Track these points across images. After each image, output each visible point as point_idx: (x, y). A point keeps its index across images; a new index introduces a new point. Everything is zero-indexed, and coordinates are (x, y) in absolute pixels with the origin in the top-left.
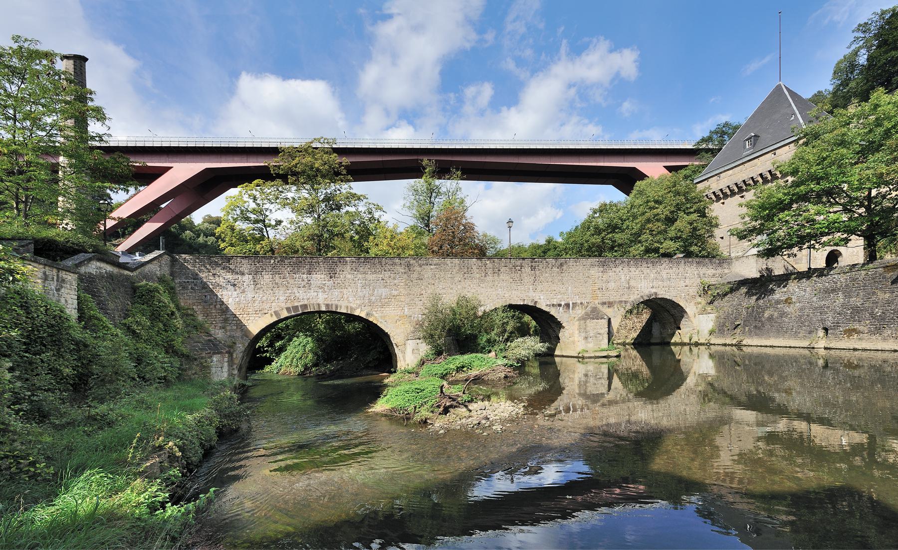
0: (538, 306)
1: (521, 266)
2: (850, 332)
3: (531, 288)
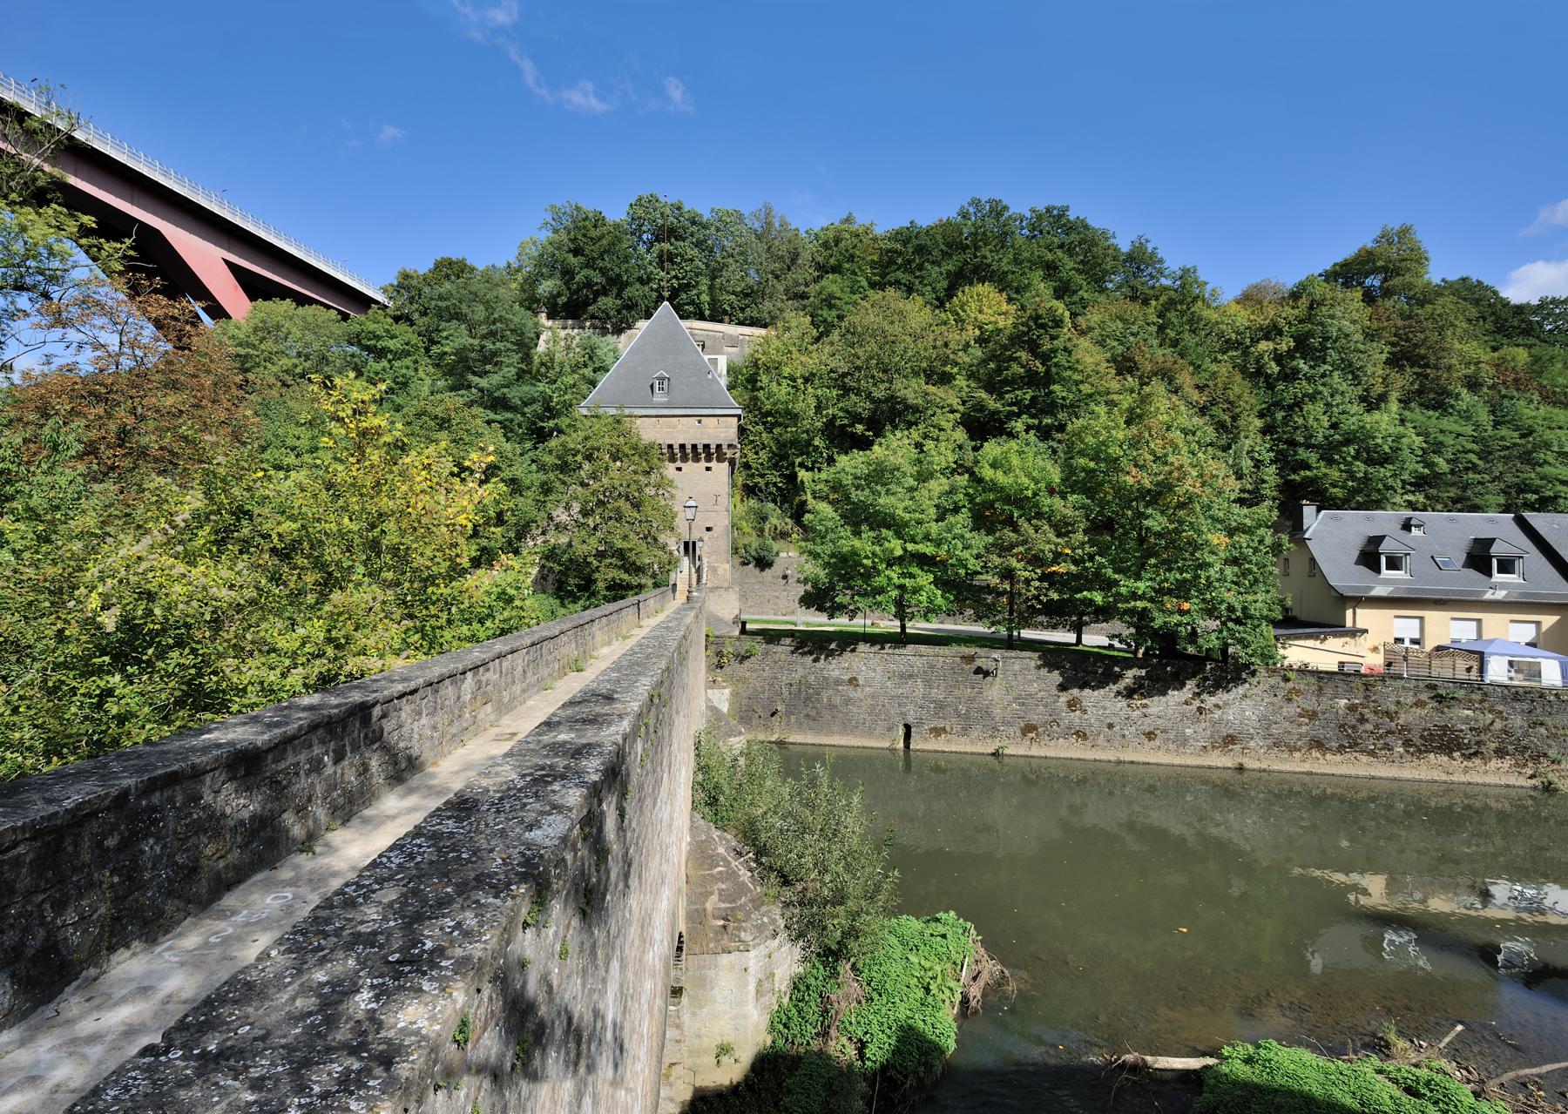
2: (938, 732)
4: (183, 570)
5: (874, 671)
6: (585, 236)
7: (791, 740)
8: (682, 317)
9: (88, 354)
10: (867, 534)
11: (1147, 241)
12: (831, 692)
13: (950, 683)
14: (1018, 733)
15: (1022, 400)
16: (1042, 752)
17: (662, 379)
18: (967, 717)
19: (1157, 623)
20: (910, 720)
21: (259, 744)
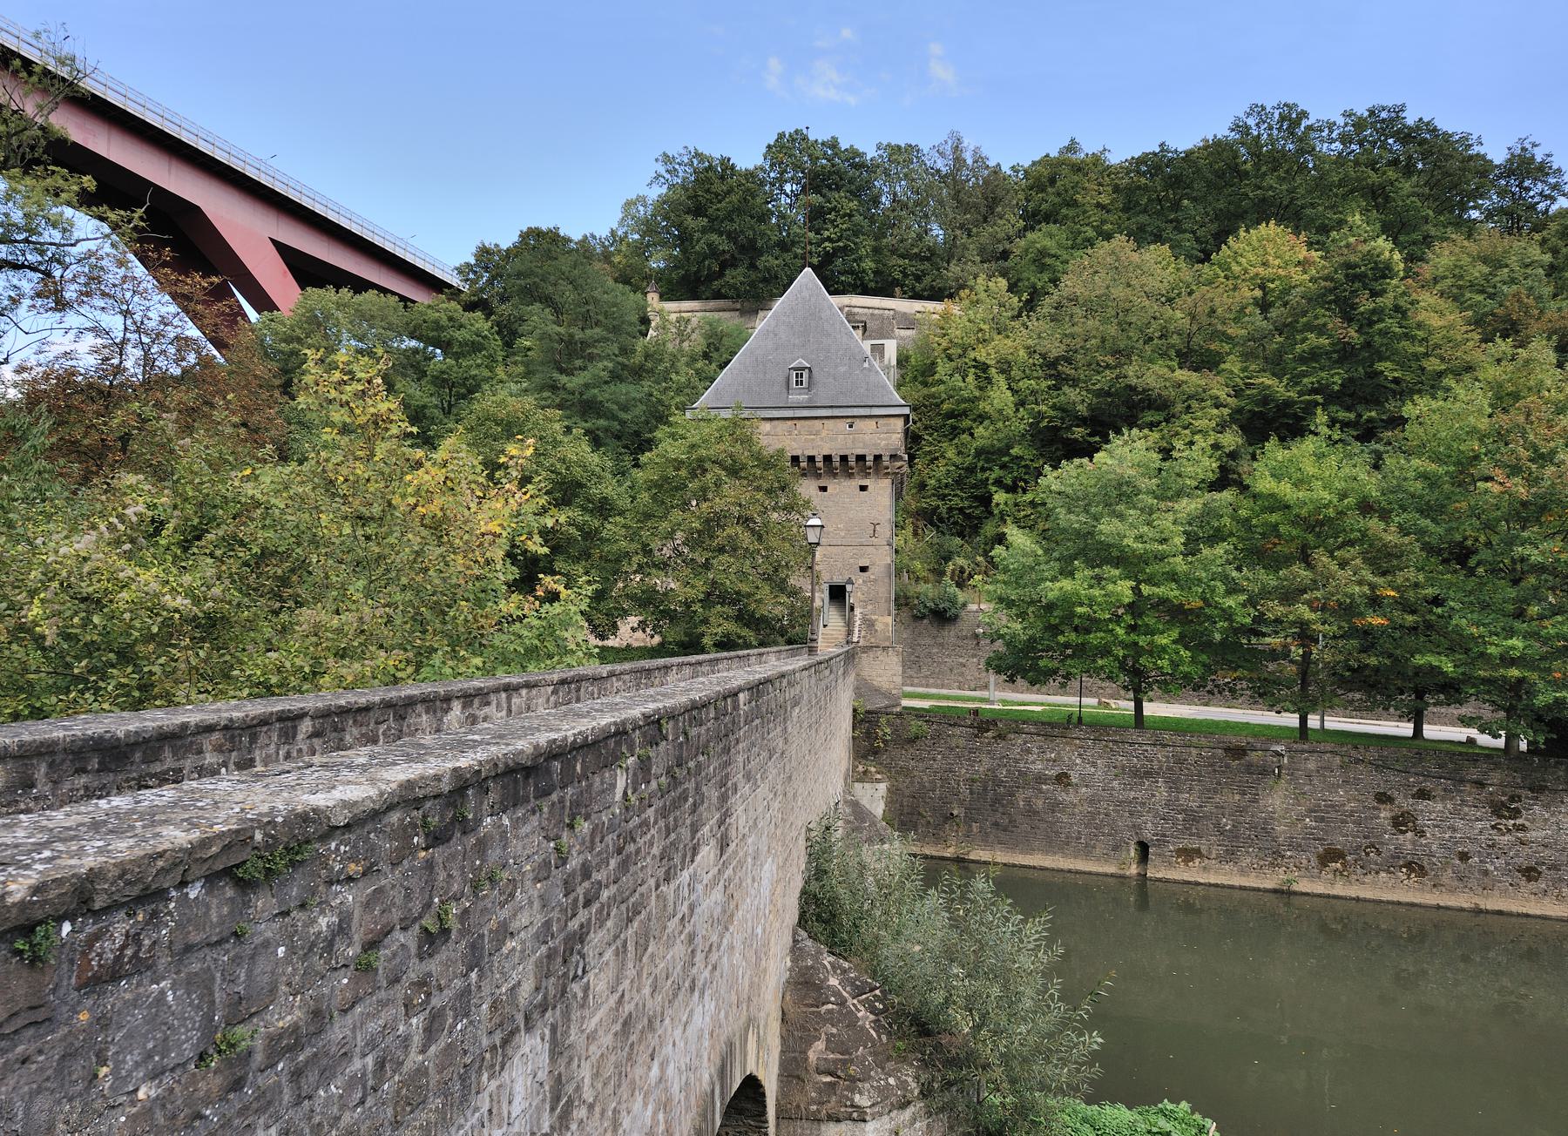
2: (1188, 855)
4: (130, 573)
5: (1094, 765)
6: (708, 191)
7: (972, 857)
8: (833, 292)
9: (90, 340)
10: (1084, 573)
11: (1534, 145)
12: (1029, 793)
13: (1208, 785)
14: (1314, 862)
15: (1328, 386)
16: (1353, 891)
17: (800, 370)
18: (1234, 835)
19: (1541, 700)
20: (1148, 835)
21: (121, 735)
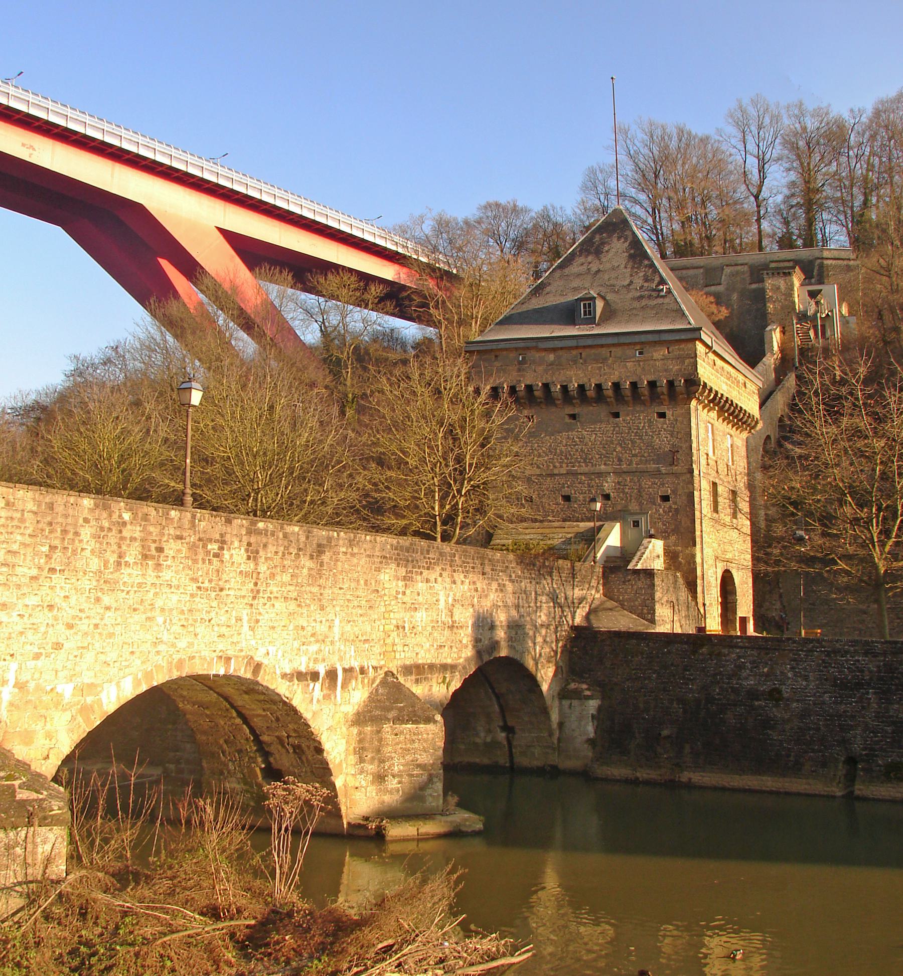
0: (264, 679)
1: (222, 542)
3: (245, 619)
5: (806, 678)
